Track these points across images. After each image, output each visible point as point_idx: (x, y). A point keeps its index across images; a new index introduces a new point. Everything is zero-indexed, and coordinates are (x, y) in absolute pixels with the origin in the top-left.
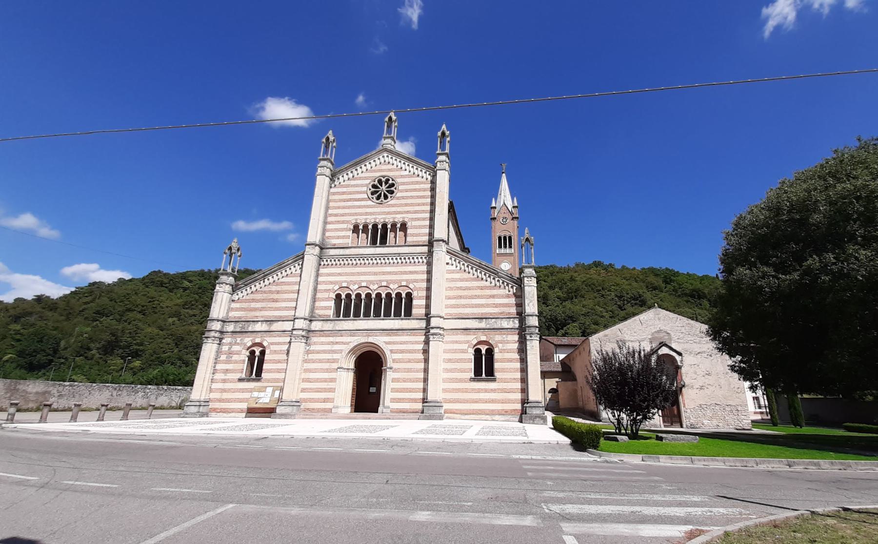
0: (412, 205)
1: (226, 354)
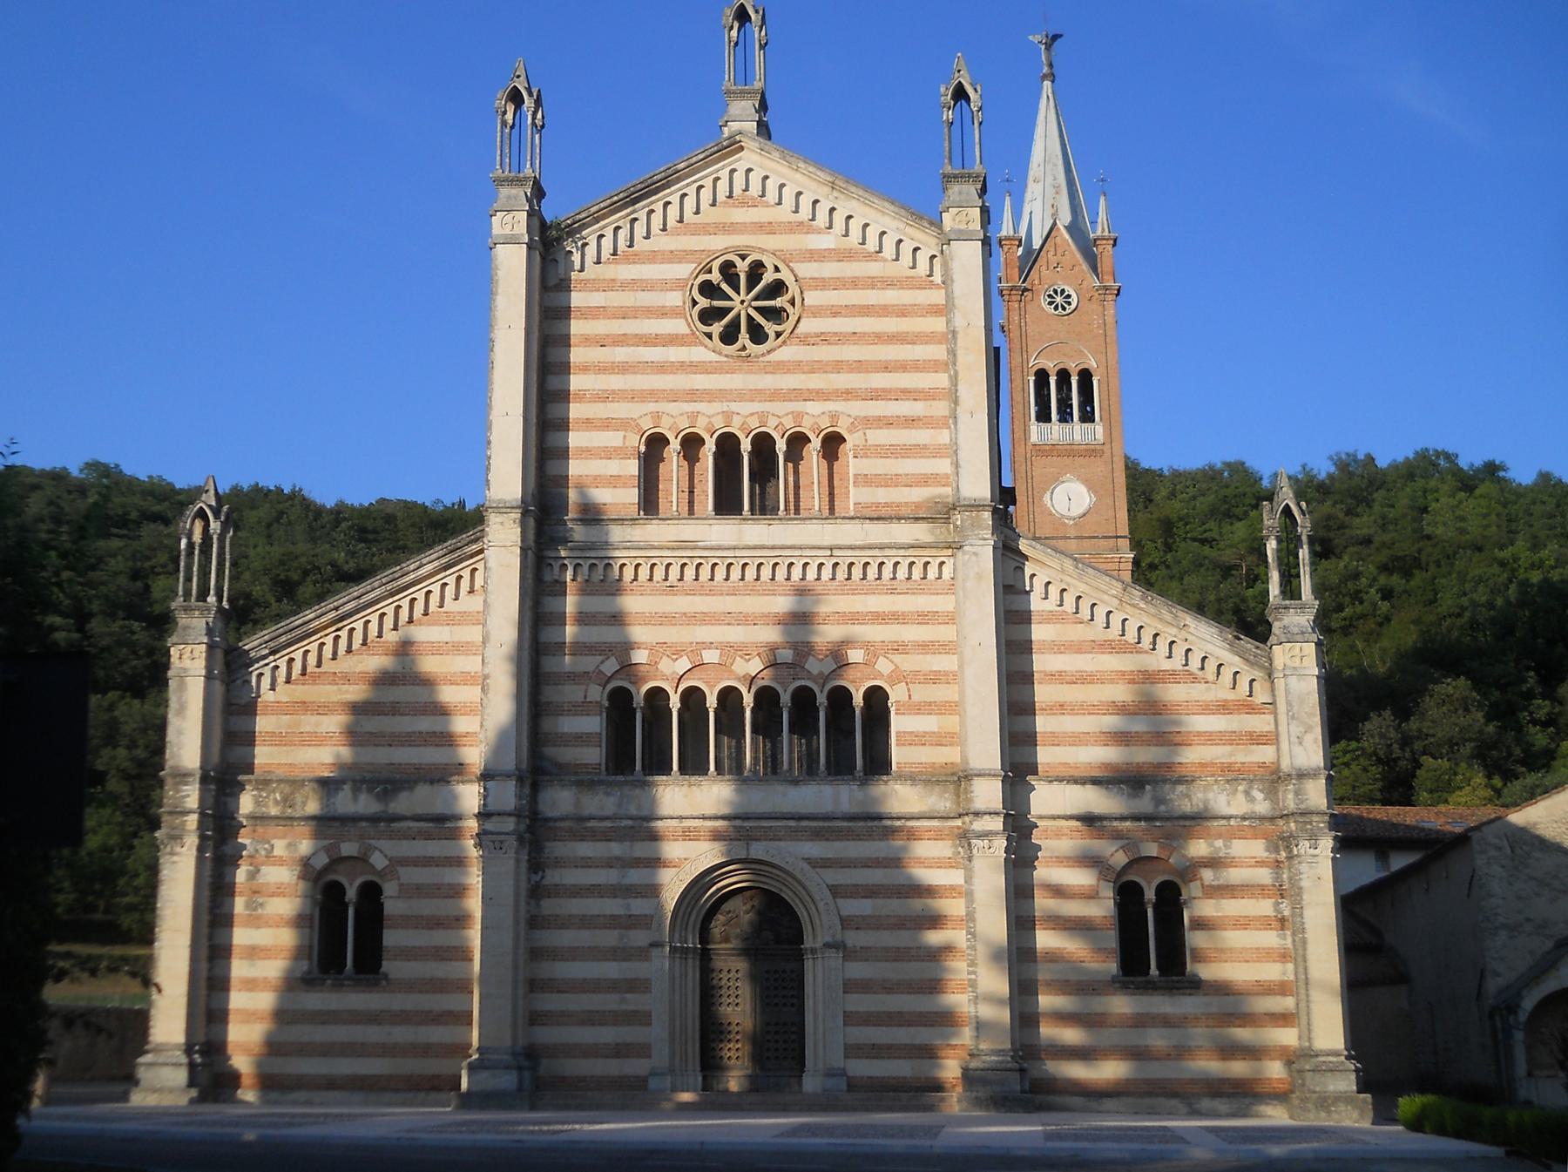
0: (859, 366)
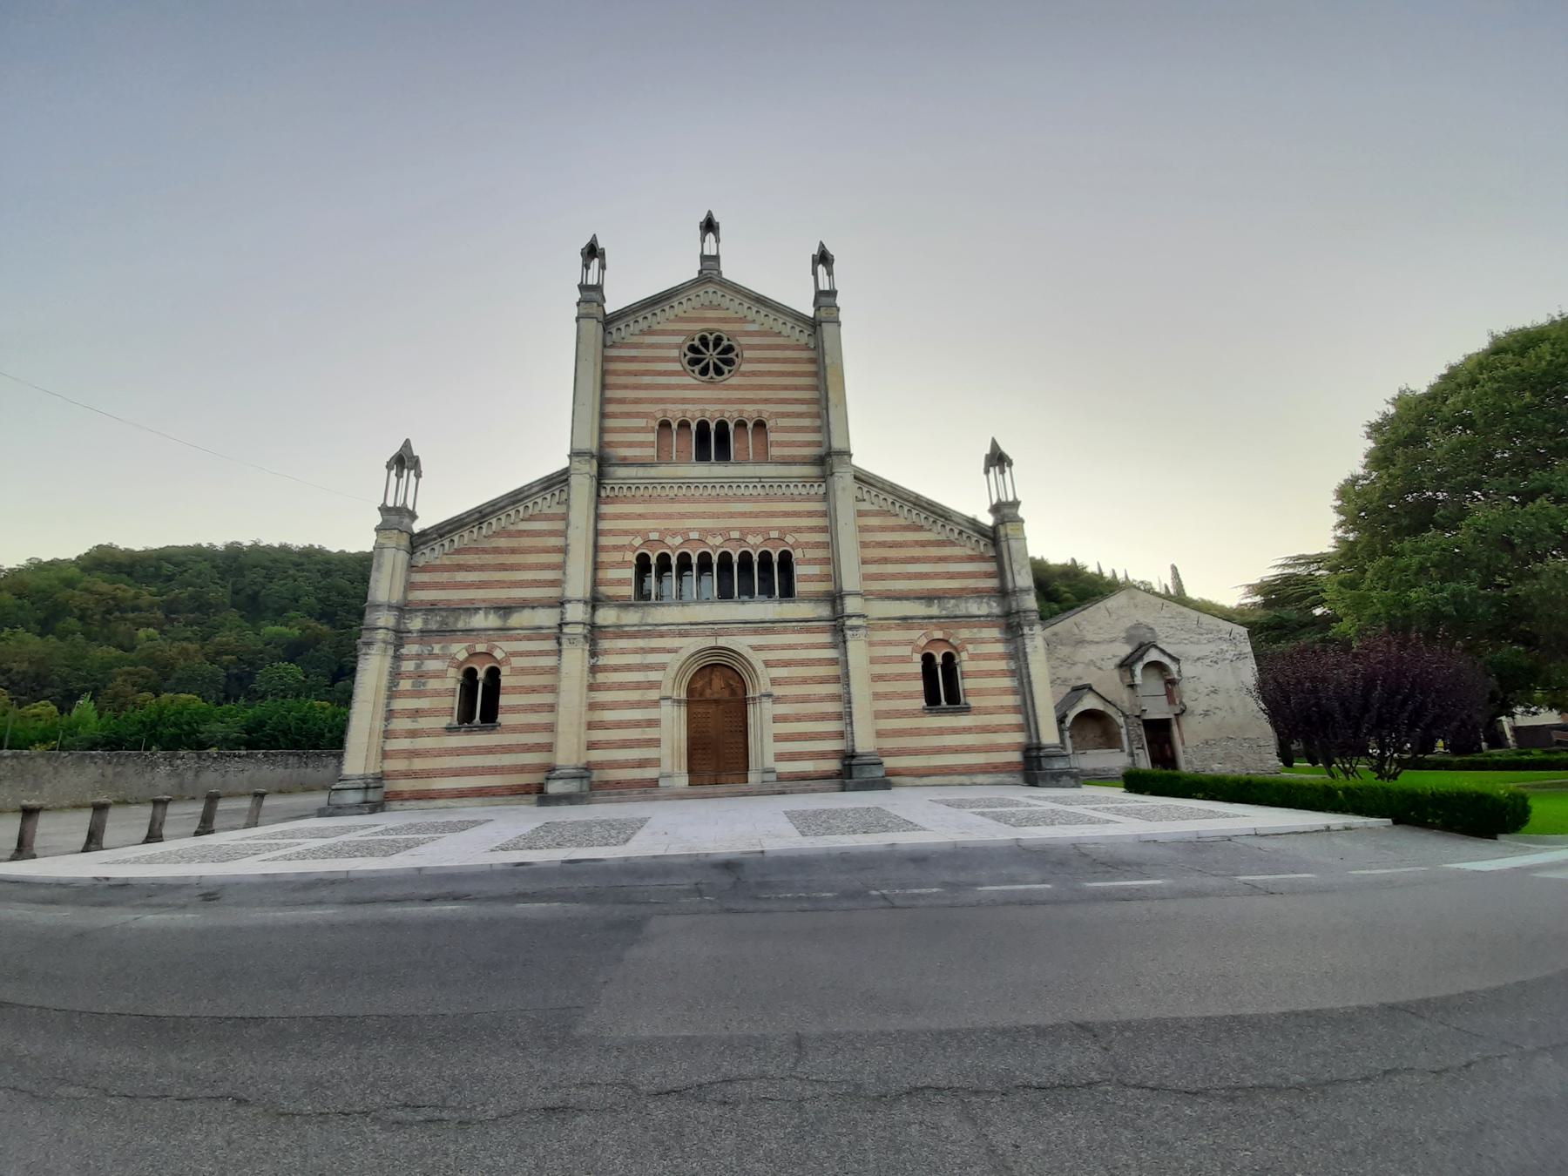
1: (409, 677)
